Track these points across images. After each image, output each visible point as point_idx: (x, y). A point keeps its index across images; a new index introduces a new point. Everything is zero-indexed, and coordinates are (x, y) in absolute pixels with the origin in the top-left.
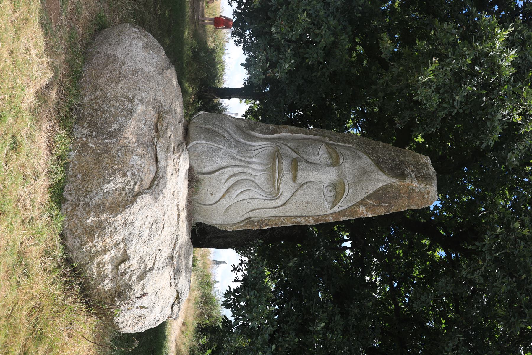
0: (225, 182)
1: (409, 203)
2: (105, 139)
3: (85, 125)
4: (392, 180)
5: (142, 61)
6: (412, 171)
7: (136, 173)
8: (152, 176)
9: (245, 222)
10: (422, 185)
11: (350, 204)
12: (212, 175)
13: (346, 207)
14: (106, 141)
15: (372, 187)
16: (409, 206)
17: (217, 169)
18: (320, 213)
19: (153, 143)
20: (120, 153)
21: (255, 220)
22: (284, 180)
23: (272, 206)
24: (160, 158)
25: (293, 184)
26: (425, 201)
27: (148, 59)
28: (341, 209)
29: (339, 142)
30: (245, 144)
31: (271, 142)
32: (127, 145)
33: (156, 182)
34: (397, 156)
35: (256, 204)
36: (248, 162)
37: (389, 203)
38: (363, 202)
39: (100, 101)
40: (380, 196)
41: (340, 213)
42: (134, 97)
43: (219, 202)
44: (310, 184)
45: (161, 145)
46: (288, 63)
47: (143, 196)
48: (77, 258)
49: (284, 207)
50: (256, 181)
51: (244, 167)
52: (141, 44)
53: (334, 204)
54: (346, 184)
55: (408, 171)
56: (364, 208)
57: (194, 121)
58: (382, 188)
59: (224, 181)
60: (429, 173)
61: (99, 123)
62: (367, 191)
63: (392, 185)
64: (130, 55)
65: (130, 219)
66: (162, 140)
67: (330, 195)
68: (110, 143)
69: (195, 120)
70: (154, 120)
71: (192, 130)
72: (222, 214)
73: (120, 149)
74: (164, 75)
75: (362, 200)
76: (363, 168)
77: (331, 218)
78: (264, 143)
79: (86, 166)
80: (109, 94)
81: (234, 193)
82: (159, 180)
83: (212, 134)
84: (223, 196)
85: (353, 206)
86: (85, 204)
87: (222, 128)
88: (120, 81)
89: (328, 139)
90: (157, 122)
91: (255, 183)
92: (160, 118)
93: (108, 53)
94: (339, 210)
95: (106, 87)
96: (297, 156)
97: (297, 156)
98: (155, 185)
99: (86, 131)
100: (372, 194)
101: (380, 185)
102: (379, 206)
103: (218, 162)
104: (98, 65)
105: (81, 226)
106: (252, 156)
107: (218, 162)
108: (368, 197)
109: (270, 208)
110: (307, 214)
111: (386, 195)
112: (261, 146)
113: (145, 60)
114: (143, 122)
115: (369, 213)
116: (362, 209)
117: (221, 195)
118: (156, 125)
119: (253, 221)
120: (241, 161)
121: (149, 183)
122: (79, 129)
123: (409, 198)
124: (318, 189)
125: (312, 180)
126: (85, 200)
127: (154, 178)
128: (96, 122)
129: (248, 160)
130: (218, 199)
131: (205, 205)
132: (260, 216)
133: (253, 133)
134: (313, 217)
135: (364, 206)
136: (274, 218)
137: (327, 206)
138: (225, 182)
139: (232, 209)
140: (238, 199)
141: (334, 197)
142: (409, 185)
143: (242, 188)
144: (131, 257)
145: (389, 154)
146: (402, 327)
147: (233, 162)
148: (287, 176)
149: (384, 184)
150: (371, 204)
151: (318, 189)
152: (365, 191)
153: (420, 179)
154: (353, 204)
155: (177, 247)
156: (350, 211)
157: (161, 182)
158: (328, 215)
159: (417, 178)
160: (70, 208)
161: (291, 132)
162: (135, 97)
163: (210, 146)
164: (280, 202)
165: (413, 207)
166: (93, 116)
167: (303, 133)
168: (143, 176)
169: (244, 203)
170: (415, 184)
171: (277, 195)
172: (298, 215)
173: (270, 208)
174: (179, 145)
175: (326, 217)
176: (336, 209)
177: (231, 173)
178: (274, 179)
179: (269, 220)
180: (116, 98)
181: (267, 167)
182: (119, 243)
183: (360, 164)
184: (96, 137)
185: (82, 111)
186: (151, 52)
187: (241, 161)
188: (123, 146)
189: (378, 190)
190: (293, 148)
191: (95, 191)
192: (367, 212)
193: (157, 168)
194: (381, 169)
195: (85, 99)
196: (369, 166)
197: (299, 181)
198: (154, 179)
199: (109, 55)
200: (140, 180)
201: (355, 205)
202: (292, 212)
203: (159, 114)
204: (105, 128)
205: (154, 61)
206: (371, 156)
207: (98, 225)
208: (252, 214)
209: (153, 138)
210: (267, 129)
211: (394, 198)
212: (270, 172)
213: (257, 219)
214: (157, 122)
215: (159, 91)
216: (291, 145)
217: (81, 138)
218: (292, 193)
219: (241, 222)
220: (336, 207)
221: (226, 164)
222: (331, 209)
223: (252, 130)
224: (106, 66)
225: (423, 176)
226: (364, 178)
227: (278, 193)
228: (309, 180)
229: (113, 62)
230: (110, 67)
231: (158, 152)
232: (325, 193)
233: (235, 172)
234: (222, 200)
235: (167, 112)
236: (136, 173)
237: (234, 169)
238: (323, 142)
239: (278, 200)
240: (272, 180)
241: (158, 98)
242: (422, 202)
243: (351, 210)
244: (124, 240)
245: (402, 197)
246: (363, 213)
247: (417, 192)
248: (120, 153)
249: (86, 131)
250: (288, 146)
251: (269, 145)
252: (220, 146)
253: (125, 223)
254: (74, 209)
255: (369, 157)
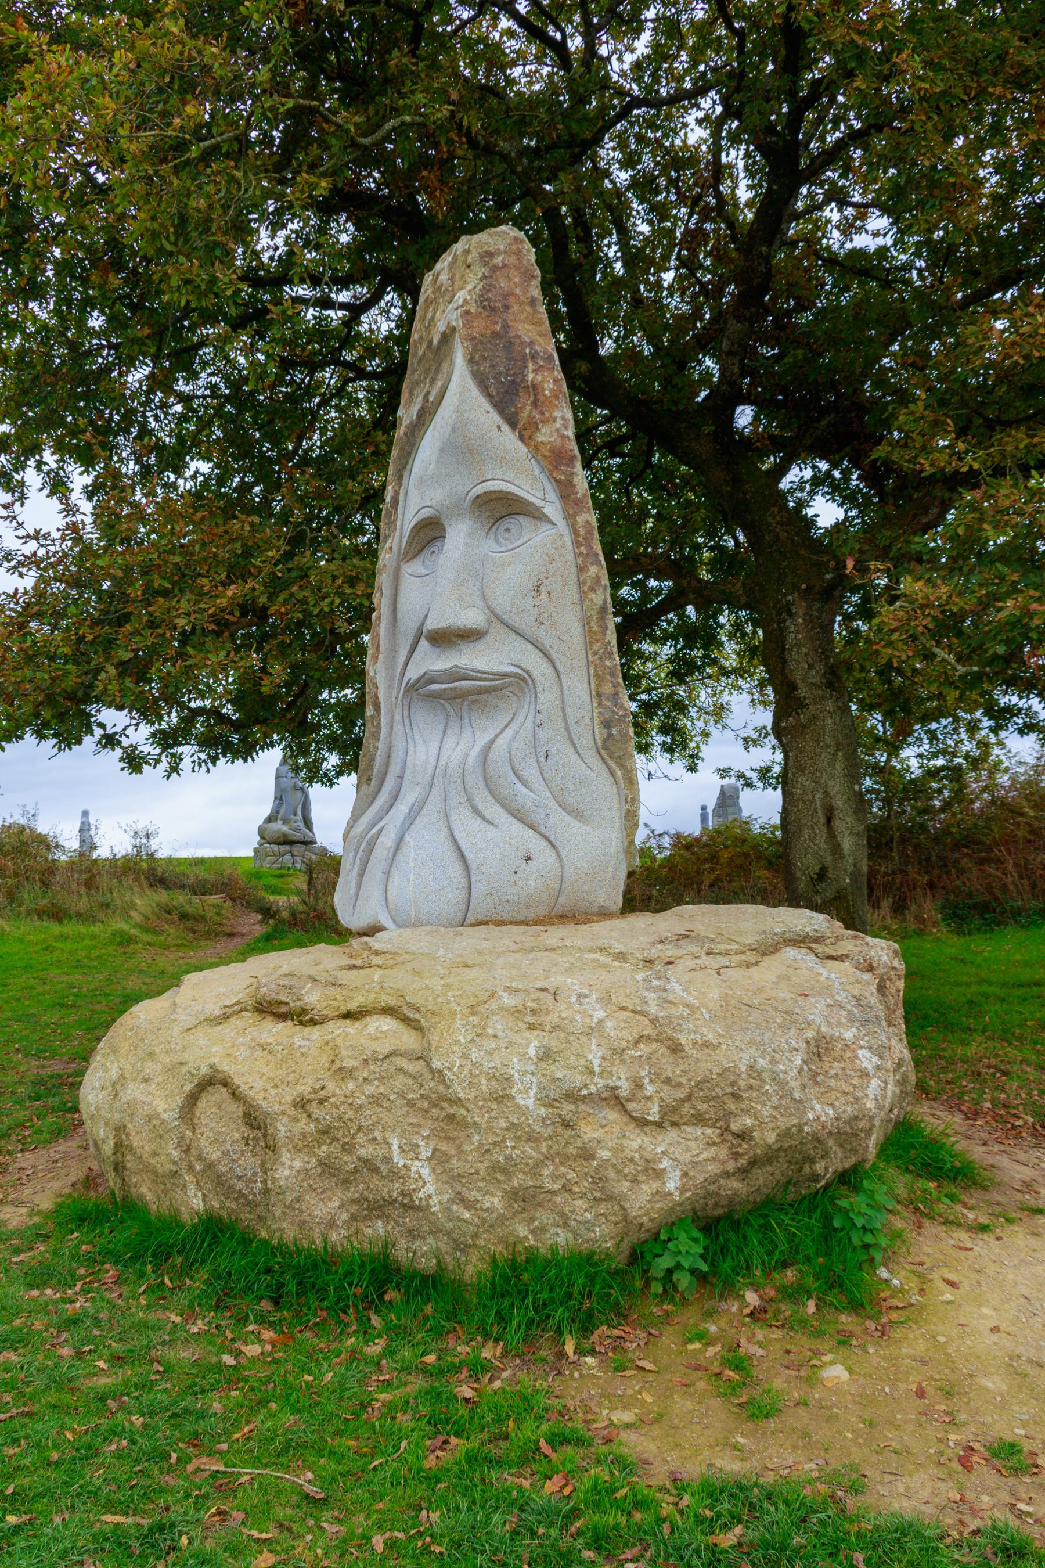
0: (488, 822)
16: (533, 302)
21: (600, 733)
25: (489, 638)
28: (552, 496)
38: (526, 434)
40: (507, 396)
41: (565, 490)
46: (56, 262)
54: (479, 490)
75: (521, 438)
81: (521, 800)
115: (558, 414)
116: (545, 435)
119: (605, 741)
132: (587, 721)
140: (539, 784)
146: (1035, 149)
155: (353, 962)
164: (538, 667)
165: (536, 292)
171: (524, 680)
176: (553, 509)
178: (481, 691)
208: (586, 742)
218: (514, 636)
219: (613, 774)
239: (535, 673)
240: (483, 697)
242: (518, 268)
243: (554, 461)
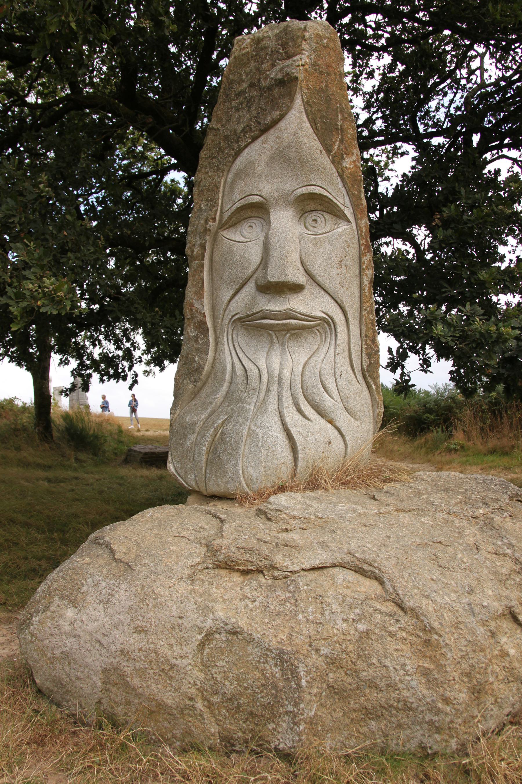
0: (308, 419)
1: (335, 74)
2: (299, 685)
3: (270, 727)
4: (298, 101)
5: (110, 611)
6: (273, 65)
7: (357, 611)
8: (351, 576)
9: (370, 381)
10: (305, 45)
11: (341, 185)
12: (298, 444)
13: (345, 193)
14: (303, 682)
15: (310, 141)
17: (286, 436)
18: (356, 241)
19: (286, 577)
20: (325, 651)
22: (302, 309)
23: (346, 331)
24: (316, 563)
26: (331, 45)
27: (102, 597)
28: (348, 203)
29: (216, 203)
30: (231, 383)
31: (222, 332)
32: (306, 637)
33: (365, 567)
34: (239, 94)
35: (343, 361)
36: (270, 375)
37: (337, 113)
38: (337, 160)
39: (216, 699)
41: (355, 206)
42: (200, 630)
43: (342, 430)
44: (306, 260)
45: (287, 563)
47: (400, 592)
48: (514, 704)
49: (347, 309)
50: (303, 361)
51: (280, 384)
52: (70, 613)
53: (337, 214)
55: (274, 74)
56: (346, 160)
57: (193, 483)
58: (313, 122)
59: (307, 421)
60: (276, 36)
61: (265, 701)
62: (318, 151)
63: (306, 104)
64: (99, 637)
65: (448, 616)
66: (279, 559)
67: (324, 224)
68: (308, 672)
69: (190, 481)
70: (237, 578)
71: (214, 488)
72: (359, 423)
73: (317, 651)
74: (129, 558)
75: (333, 162)
76: (271, 158)
77: (363, 221)
78: (226, 347)
79: (354, 716)
80: (198, 683)
81: (327, 403)
82: (359, 560)
83: (221, 448)
84: (331, 422)
85: (343, 180)
86: (430, 710)
87: (205, 428)
88: (168, 660)
89: (211, 223)
90: (238, 570)
91: (306, 363)
92: (228, 566)
93: (99, 684)
94: (350, 206)
95: (184, 689)
96: (251, 284)
97: (251, 284)
98: (373, 569)
99: (284, 725)
100: (323, 142)
101: (308, 125)
102: (342, 130)
103: (274, 434)
104: (128, 703)
105: (468, 711)
106: (256, 371)
107: (274, 434)
108: (328, 151)
109: (349, 335)
110: (357, 266)
111: (324, 116)
112: (236, 355)
113: (106, 603)
114: (250, 605)
117: (329, 426)
118: (245, 573)
119: (368, 366)
120: (268, 390)
121: (367, 582)
122: (279, 736)
123: (328, 74)
124: (316, 244)
125: (298, 254)
126: (422, 712)
127: (356, 571)
128: (264, 707)
129: (265, 378)
130: (337, 433)
131: (346, 454)
132: (360, 353)
133: (206, 368)
134: (361, 255)
135: (343, 158)
136: (364, 328)
137: (342, 228)
138: (308, 419)
139: (351, 405)
141: (325, 214)
142: (306, 70)
143: (318, 388)
144: (506, 602)
145: (237, 110)
147: (273, 407)
148: (295, 303)
149: (305, 118)
150: (339, 146)
151: (316, 244)
152: (317, 155)
153: (290, 50)
154: (339, 180)
156: (353, 186)
157: (362, 556)
158: (358, 226)
159: (289, 57)
160: (436, 736)
161: (200, 295)
162: (199, 628)
163: (247, 451)
164: (338, 317)
166: (251, 714)
167: (202, 272)
168: (362, 597)
169: (342, 383)
170: (304, 58)
172: (358, 283)
173: (349, 335)
174: (269, 519)
175: (362, 232)
176: (349, 213)
177: (293, 410)
179: (366, 336)
180: (205, 667)
181: (276, 341)
182: (490, 631)
183: (263, 163)
184: (296, 705)
185: (240, 734)
186: (84, 589)
187: (268, 390)
188: (310, 646)
189: (316, 130)
190: (232, 291)
191: (406, 693)
192: (353, 154)
193: (336, 566)
194: (275, 122)
195: (212, 730)
196: (266, 146)
197: (301, 278)
198: (359, 571)
199: (103, 683)
200: (370, 603)
201: (341, 176)
202: (354, 294)
203: (218, 567)
204: (275, 686)
205: (103, 584)
206: (243, 144)
207: (466, 679)
209: (275, 578)
210: (196, 341)
211: (328, 100)
212: (285, 335)
213: (365, 359)
214: (238, 570)
215: (171, 570)
216: (226, 294)
217: (299, 734)
218: (323, 293)
220: (346, 212)
221: (277, 419)
222: (349, 221)
223: (199, 370)
224: (134, 689)
225: (284, 46)
226: (294, 155)
227: (323, 319)
228: (299, 260)
229: (122, 676)
230: (136, 682)
231: (304, 566)
232: (320, 232)
233: (291, 402)
234: (338, 424)
235: (212, 550)
236: (357, 611)
237: (285, 404)
238: (216, 233)
241: (187, 572)
244: (484, 623)
245: (326, 86)
246: (354, 162)
247: (319, 57)
248: (325, 651)
249: (284, 725)
250: (230, 301)
251: (230, 338)
252: (245, 432)
253: (456, 625)
254: (439, 730)
255: (246, 147)
